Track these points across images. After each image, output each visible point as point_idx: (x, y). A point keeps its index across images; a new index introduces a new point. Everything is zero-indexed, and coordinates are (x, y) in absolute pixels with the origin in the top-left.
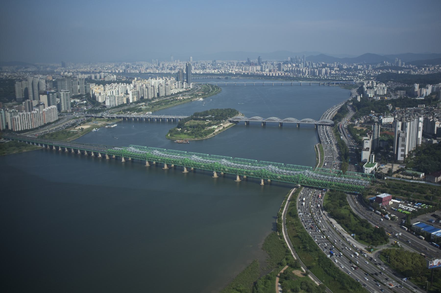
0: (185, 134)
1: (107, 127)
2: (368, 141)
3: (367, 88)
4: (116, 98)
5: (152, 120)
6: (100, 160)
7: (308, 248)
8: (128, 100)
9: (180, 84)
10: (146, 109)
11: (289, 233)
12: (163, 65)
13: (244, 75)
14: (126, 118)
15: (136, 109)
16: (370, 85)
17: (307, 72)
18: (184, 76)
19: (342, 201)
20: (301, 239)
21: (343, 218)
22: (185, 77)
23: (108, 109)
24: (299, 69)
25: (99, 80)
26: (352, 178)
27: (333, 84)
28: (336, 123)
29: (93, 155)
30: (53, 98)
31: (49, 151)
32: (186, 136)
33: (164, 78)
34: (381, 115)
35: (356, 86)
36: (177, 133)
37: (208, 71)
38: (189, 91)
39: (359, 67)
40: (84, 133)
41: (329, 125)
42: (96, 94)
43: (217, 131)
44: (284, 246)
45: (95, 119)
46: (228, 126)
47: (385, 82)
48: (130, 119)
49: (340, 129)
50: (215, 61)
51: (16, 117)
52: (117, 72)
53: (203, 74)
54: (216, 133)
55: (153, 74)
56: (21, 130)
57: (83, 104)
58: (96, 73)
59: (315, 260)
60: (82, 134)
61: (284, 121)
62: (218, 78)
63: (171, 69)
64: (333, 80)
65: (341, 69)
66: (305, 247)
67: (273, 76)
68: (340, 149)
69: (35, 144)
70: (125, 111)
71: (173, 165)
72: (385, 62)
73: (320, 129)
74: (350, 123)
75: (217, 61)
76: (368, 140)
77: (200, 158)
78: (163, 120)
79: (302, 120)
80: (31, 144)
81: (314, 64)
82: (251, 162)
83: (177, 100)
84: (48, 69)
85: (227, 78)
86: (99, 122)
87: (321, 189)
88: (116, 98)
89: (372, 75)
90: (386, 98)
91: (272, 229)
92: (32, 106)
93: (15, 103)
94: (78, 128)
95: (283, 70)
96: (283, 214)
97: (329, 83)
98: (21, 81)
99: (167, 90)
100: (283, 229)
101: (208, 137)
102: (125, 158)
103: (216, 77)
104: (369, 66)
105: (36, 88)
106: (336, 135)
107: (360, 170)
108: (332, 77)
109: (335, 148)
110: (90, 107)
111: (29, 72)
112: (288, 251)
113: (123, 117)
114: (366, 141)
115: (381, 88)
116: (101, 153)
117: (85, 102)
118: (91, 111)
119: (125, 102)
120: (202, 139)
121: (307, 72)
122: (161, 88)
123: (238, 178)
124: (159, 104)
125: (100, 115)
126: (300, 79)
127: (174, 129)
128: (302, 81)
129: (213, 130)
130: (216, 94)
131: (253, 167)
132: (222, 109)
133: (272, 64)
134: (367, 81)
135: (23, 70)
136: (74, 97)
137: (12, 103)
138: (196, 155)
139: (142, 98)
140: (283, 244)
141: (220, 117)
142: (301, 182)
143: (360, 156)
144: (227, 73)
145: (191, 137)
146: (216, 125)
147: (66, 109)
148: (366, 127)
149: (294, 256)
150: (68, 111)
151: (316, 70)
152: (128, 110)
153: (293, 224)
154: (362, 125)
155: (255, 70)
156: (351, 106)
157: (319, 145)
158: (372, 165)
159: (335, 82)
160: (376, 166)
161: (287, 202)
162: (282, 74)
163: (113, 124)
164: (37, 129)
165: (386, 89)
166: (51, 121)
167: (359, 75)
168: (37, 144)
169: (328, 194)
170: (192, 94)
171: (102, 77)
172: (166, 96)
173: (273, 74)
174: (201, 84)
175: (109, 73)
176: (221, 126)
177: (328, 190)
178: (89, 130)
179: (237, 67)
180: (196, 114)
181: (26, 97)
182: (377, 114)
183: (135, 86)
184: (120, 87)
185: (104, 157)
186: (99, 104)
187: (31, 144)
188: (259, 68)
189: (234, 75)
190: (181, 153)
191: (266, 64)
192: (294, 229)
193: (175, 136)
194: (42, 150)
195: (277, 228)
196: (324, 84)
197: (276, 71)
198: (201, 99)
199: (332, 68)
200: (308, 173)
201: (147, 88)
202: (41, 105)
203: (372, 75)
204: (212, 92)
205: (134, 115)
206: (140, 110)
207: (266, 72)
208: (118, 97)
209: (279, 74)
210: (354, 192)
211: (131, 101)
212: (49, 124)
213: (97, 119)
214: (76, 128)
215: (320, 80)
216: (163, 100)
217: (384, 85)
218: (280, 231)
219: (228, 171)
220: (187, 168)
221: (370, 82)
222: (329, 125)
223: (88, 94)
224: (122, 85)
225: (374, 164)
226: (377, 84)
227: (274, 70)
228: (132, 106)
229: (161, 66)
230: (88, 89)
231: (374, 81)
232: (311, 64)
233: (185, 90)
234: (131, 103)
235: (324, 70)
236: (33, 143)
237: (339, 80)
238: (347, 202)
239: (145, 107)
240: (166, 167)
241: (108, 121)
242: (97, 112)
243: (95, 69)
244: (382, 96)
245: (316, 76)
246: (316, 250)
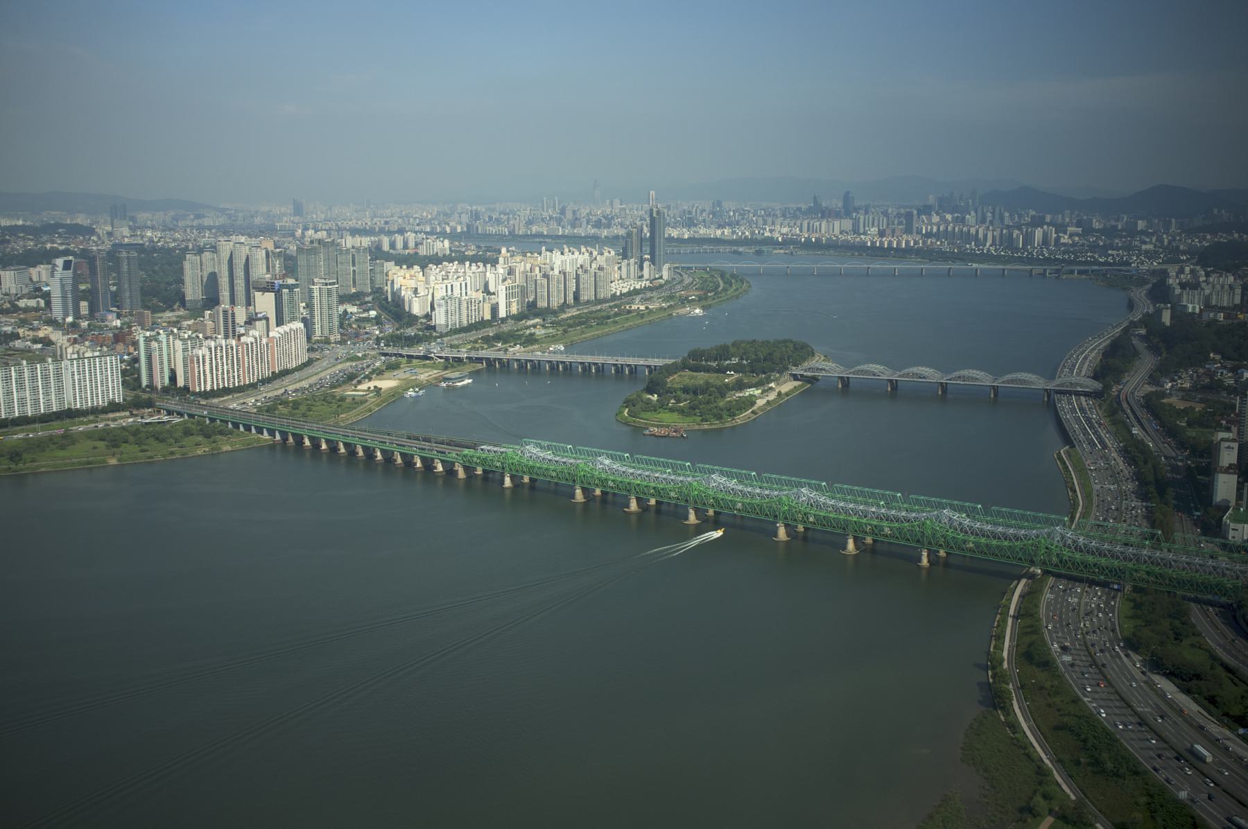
0: (672, 410)
1: (444, 385)
3: (1183, 286)
4: (464, 305)
5: (569, 368)
6: (440, 482)
7: (1109, 765)
8: (495, 309)
9: (632, 268)
10: (547, 336)
11: (1033, 714)
12: (574, 212)
13: (808, 245)
14: (495, 360)
15: (520, 337)
17: (989, 237)
18: (642, 244)
19: (1177, 623)
20: (1078, 735)
21: (1198, 677)
22: (647, 249)
23: (441, 336)
24: (965, 229)
25: (402, 252)
27: (1072, 272)
28: (1107, 387)
29: (324, 446)
30: (291, 301)
31: (292, 448)
32: (675, 416)
33: (583, 249)
35: (1141, 282)
36: (649, 407)
37: (702, 231)
38: (661, 286)
39: (1141, 225)
40: (383, 402)
41: (1086, 394)
42: (403, 293)
43: (761, 402)
44: (1028, 756)
45: (409, 362)
46: (792, 391)
48: (505, 365)
49: (1125, 405)
50: (719, 204)
51: (200, 353)
52: (448, 230)
53: (691, 240)
54: (760, 408)
55: (547, 236)
56: (212, 390)
57: (368, 320)
58: (394, 233)
59: (1137, 804)
60: (378, 405)
61: (903, 376)
62: (735, 252)
63: (598, 224)
64: (1070, 262)
65: (1088, 231)
66: (1097, 762)
67: (890, 248)
68: (1136, 465)
69: (253, 431)
70: (488, 340)
71: (653, 502)
72: (1215, 211)
73: (1063, 405)
74: (1149, 389)
75: (726, 205)
77: (733, 483)
78: (601, 369)
79: (953, 375)
80: (242, 429)
81: (1007, 214)
82: (883, 497)
83: (629, 312)
84: (258, 220)
85: (759, 253)
86: (422, 370)
87: (1104, 585)
88: (464, 305)
89: (1182, 247)
90: (1241, 316)
91: (980, 702)
92: (233, 322)
93: (182, 312)
94: (364, 386)
95: (919, 232)
96: (1005, 654)
97: (1058, 271)
98: (200, 251)
99: (600, 284)
100: (1015, 703)
101: (740, 422)
102: (512, 477)
103: (728, 249)
104: (1170, 222)
105: (239, 273)
106: (1114, 423)
107: (1212, 527)
108: (1064, 253)
109: (1121, 464)
110: (389, 329)
111: (210, 228)
112: (1041, 772)
113: (488, 359)
114: (1227, 444)
115: (1223, 287)
116: (442, 461)
117: (373, 313)
118: (394, 340)
119: (488, 316)
120: (720, 426)
121: (989, 237)
122: (583, 277)
123: (851, 545)
124: (581, 324)
125: (421, 350)
126: (973, 257)
127: (639, 396)
128: (979, 262)
129: (751, 401)
130: (737, 297)
131: (893, 512)
132: (768, 342)
133: (885, 214)
134: (1177, 267)
135: (190, 224)
136: (343, 299)
137: (177, 313)
138: (722, 473)
139: (532, 305)
140: (1025, 748)
141: (765, 361)
142: (930, 543)
143: (1209, 488)
144: (759, 237)
145: (691, 419)
146: (756, 386)
147: (326, 333)
148: (1201, 401)
149: (1065, 787)
150: (332, 338)
151: (1016, 232)
152: (498, 338)
153: (1042, 688)
154: (1187, 394)
155: (837, 231)
156: (1144, 338)
157: (1067, 452)
159: (1077, 268)
161: (1010, 620)
162: (916, 242)
163: (461, 379)
164: (253, 386)
165: (1238, 291)
166: (289, 366)
167: (1144, 247)
168: (260, 431)
169: (1128, 599)
170: (671, 297)
171: (411, 244)
172: (598, 301)
173: (890, 243)
174: (690, 268)
175: (426, 233)
176: (771, 388)
177: (1128, 588)
178: (396, 395)
179: (786, 222)
180: (696, 355)
181: (212, 301)
182: (1229, 364)
183: (511, 272)
184: (469, 273)
185: (450, 472)
186: (413, 319)
187: (242, 429)
188: (847, 224)
189: (777, 243)
190: (672, 466)
191: (866, 212)
192: (1049, 706)
193: (643, 415)
194: (272, 447)
195: (995, 699)
196: (1044, 275)
197: (897, 233)
198: (697, 311)
199: (1061, 228)
200: (1062, 535)
201: (546, 276)
202: (260, 319)
203: (1182, 247)
204: (725, 290)
205: (517, 351)
206: (531, 340)
207: (870, 236)
208: (470, 302)
209: (907, 242)
210: (1210, 597)
211: (502, 313)
212: (285, 373)
213: (415, 361)
214: (359, 387)
215: (1030, 260)
216: (591, 312)
217: (1231, 279)
218: (1008, 711)
219: (892, 536)
220: (697, 510)
222: (1086, 394)
223: (378, 292)
224: (474, 267)
226: (1207, 275)
227: (893, 231)
228: (505, 328)
229: (569, 215)
230: (378, 279)
231: (1198, 268)
232: (997, 216)
233: (648, 284)
234: (503, 320)
235: (1038, 233)
236: (248, 428)
237: (1086, 263)
238: (1193, 626)
239: (543, 332)
240: (634, 506)
241: (446, 368)
242: (412, 341)
243: (386, 223)
244: (1229, 311)
245: (1017, 250)
246: (1136, 773)
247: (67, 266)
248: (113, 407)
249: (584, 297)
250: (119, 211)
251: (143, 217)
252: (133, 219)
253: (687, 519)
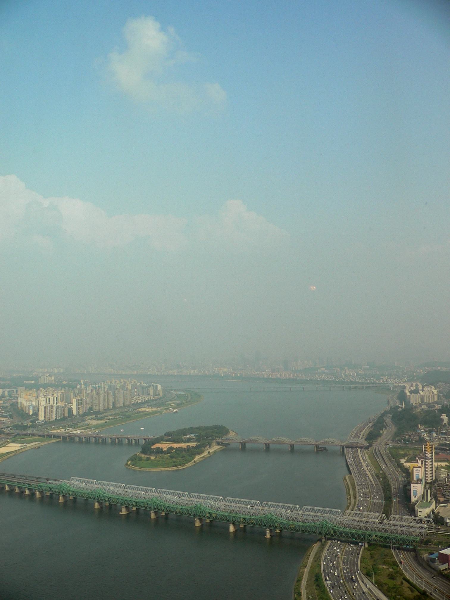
2: (418, 469)
8: (70, 411)
16: (413, 388)
26: (399, 523)
34: (433, 431)
41: (361, 447)
47: (434, 384)
76: (420, 467)
107: (412, 512)
158: (429, 504)
160: (433, 506)
162: (289, 375)
211: (75, 412)
221: (414, 385)
222: (361, 447)
225: (430, 503)
226: (423, 387)
231: (419, 384)
249: (118, 405)
253: (121, 511)
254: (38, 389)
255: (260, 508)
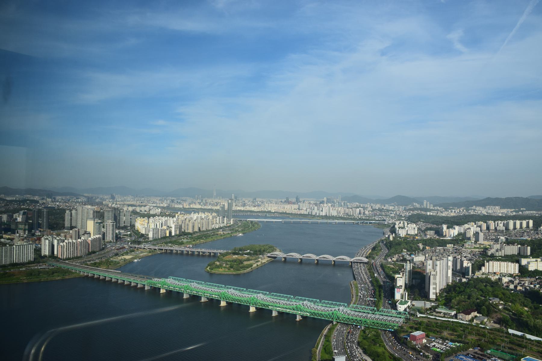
8: (170, 233)
10: (187, 242)
16: (401, 225)
18: (223, 213)
38: (230, 226)
43: (255, 265)
57: (127, 235)
64: (367, 220)
70: (166, 243)
83: (217, 234)
106: (370, 272)
107: (394, 306)
159: (368, 222)
165: (416, 229)
167: (391, 215)
170: (233, 230)
182: (409, 253)
199: (364, 208)
204: (251, 228)
205: (176, 248)
211: (173, 234)
217: (415, 225)
221: (402, 222)
225: (407, 302)
226: (408, 224)
228: (174, 239)
247: (24, 213)
248: (30, 263)
250: (51, 194)
251: (58, 198)
252: (55, 199)
254: (149, 217)
255: (293, 300)
